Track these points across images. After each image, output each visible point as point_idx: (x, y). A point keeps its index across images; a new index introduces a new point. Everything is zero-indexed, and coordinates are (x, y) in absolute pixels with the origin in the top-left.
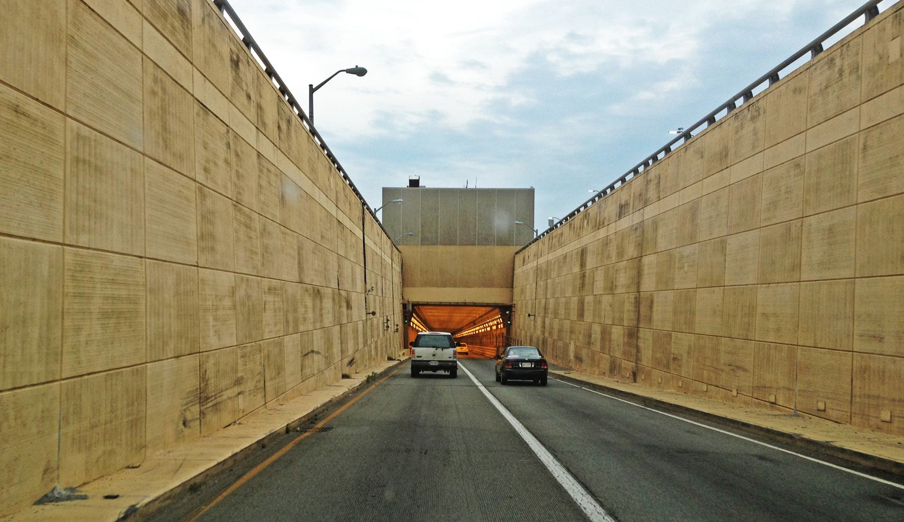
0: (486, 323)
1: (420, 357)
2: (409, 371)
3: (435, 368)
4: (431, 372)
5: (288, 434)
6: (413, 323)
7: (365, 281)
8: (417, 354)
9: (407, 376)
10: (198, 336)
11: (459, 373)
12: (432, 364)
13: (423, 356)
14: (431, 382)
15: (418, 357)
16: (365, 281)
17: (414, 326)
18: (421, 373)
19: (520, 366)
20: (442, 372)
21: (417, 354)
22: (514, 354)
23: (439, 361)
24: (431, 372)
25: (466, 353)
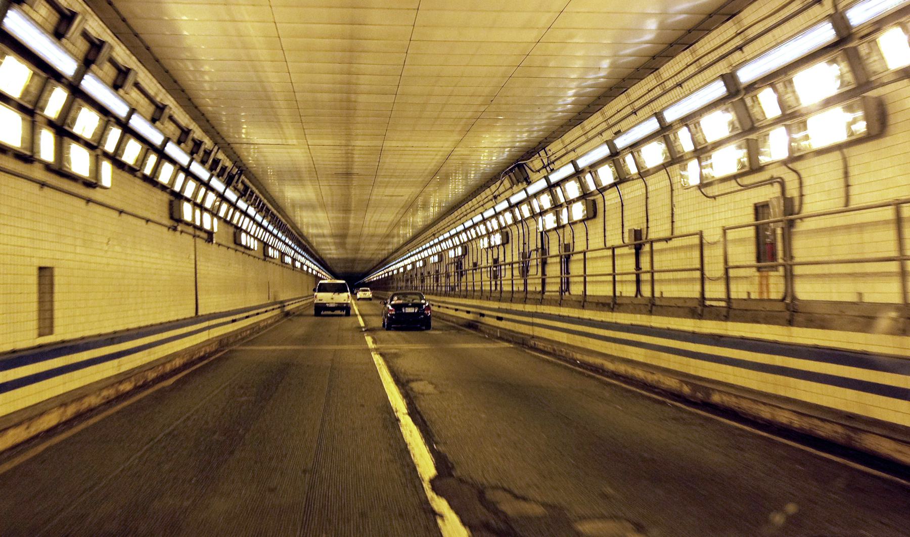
0: (512, 297)
1: (321, 300)
2: (313, 312)
3: (333, 309)
4: (330, 313)
5: (167, 116)
6: (308, 267)
7: (639, 98)
8: (318, 298)
9: (313, 316)
10: (497, 149)
11: (351, 312)
12: (331, 305)
13: (324, 299)
14: (326, 319)
15: (320, 300)
16: (639, 98)
17: (310, 270)
18: (322, 313)
19: (404, 310)
20: (338, 312)
21: (318, 298)
22: (399, 299)
23: (336, 303)
24: (330, 313)
25: (370, 299)
